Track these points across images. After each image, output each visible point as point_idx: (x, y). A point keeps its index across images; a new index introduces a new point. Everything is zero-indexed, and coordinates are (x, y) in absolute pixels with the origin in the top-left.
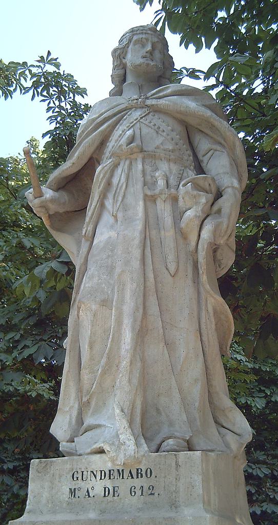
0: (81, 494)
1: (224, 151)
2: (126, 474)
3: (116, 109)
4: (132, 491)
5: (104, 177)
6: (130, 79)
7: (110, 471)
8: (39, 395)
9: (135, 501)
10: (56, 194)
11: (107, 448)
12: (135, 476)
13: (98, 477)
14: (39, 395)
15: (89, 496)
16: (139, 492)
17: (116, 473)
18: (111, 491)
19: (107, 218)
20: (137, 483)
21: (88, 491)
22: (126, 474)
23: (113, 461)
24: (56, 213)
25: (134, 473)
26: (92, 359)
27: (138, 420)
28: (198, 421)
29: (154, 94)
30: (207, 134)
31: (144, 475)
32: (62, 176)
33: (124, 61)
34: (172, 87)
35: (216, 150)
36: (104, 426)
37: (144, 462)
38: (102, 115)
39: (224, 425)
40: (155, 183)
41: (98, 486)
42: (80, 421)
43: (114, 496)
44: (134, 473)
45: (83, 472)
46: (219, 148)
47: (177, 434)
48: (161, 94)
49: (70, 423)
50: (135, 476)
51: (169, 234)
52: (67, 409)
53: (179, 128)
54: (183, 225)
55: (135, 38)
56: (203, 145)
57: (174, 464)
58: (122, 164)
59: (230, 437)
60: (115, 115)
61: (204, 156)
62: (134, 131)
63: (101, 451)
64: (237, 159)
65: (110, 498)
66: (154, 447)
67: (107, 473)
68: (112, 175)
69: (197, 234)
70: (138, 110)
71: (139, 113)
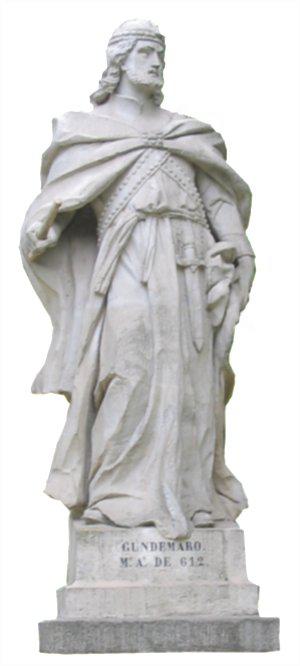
7: (161, 543)
16: (189, 563)
17: (167, 546)
20: (187, 554)
23: (163, 534)
35: (224, 202)
43: (165, 565)
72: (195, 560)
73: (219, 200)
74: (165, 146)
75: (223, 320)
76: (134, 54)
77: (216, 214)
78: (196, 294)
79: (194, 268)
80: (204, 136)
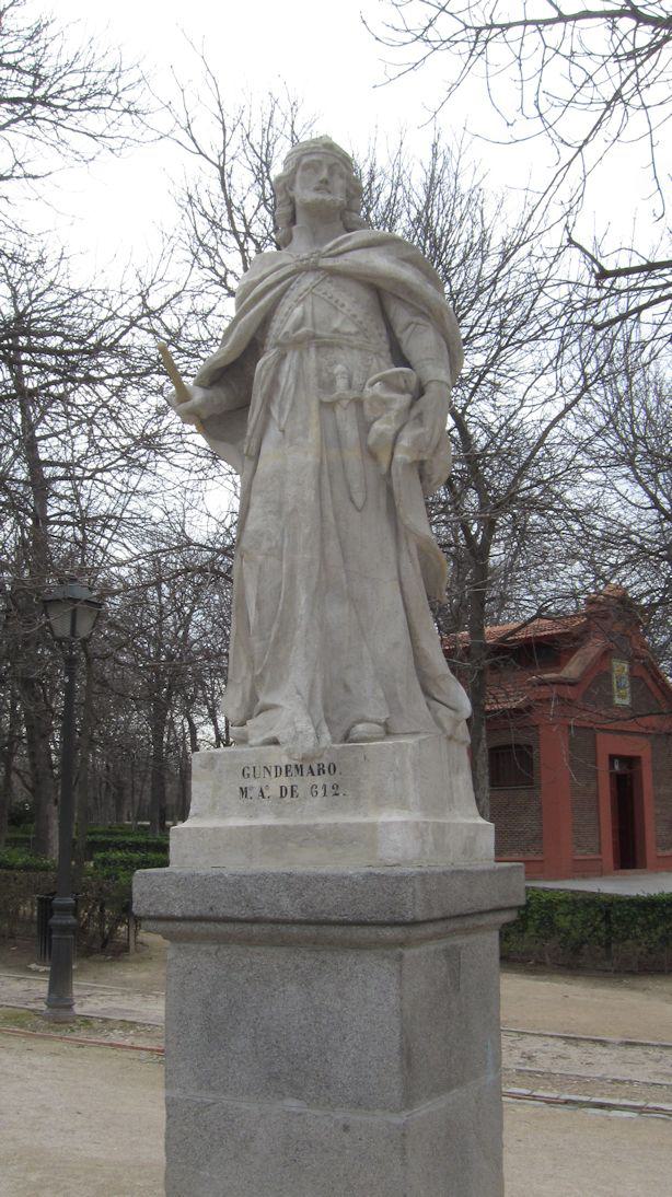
0: (254, 793)
1: (428, 324)
2: (306, 770)
3: (282, 273)
5: (267, 374)
6: (300, 217)
7: (286, 767)
10: (210, 393)
12: (316, 773)
13: (273, 774)
16: (321, 792)
17: (293, 770)
18: (289, 791)
19: (273, 433)
20: (319, 781)
21: (261, 791)
22: (306, 770)
23: (290, 754)
24: (211, 417)
25: (315, 769)
26: (260, 623)
27: (319, 701)
29: (330, 249)
30: (404, 300)
31: (327, 772)
32: (218, 366)
33: (291, 194)
34: (359, 236)
35: (417, 324)
36: (281, 707)
37: (326, 755)
38: (264, 278)
39: (436, 696)
40: (333, 382)
42: (254, 698)
43: (292, 796)
44: (315, 769)
46: (421, 320)
47: (370, 716)
48: (341, 248)
49: (243, 700)
50: (316, 773)
51: (353, 456)
52: (239, 681)
53: (366, 296)
54: (370, 442)
55: (305, 160)
56: (401, 316)
58: (289, 358)
59: (443, 712)
60: (278, 282)
61: (401, 333)
62: (304, 307)
63: (275, 742)
66: (340, 736)
67: (284, 769)
68: (277, 372)
69: (389, 453)
70: (310, 274)
71: (311, 280)
72: (329, 789)
73: (410, 324)
74: (320, 264)
75: (390, 468)
76: (299, 174)
77: (408, 341)
78: (351, 432)
79: (345, 403)
80: (382, 250)
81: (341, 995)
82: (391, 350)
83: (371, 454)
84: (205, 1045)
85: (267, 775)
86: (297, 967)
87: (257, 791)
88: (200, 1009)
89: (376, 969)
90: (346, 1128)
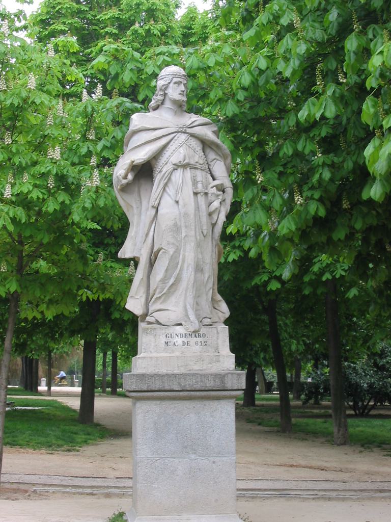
4: (196, 343)
8: (42, 102)
9: (198, 348)
11: (183, 323)
13: (179, 337)
14: (42, 102)
15: (175, 345)
18: (186, 344)
20: (199, 339)
21: (174, 343)
28: (271, 347)
35: (218, 160)
39: (217, 308)
41: (179, 341)
45: (171, 334)
57: (216, 332)
64: (219, 12)
65: (186, 346)
72: (203, 343)
81: (212, 416)
82: (164, 145)
83: (210, 214)
84: (155, 438)
85: (177, 337)
86: (194, 407)
87: (173, 344)
88: (152, 425)
89: (226, 406)
90: (214, 462)
